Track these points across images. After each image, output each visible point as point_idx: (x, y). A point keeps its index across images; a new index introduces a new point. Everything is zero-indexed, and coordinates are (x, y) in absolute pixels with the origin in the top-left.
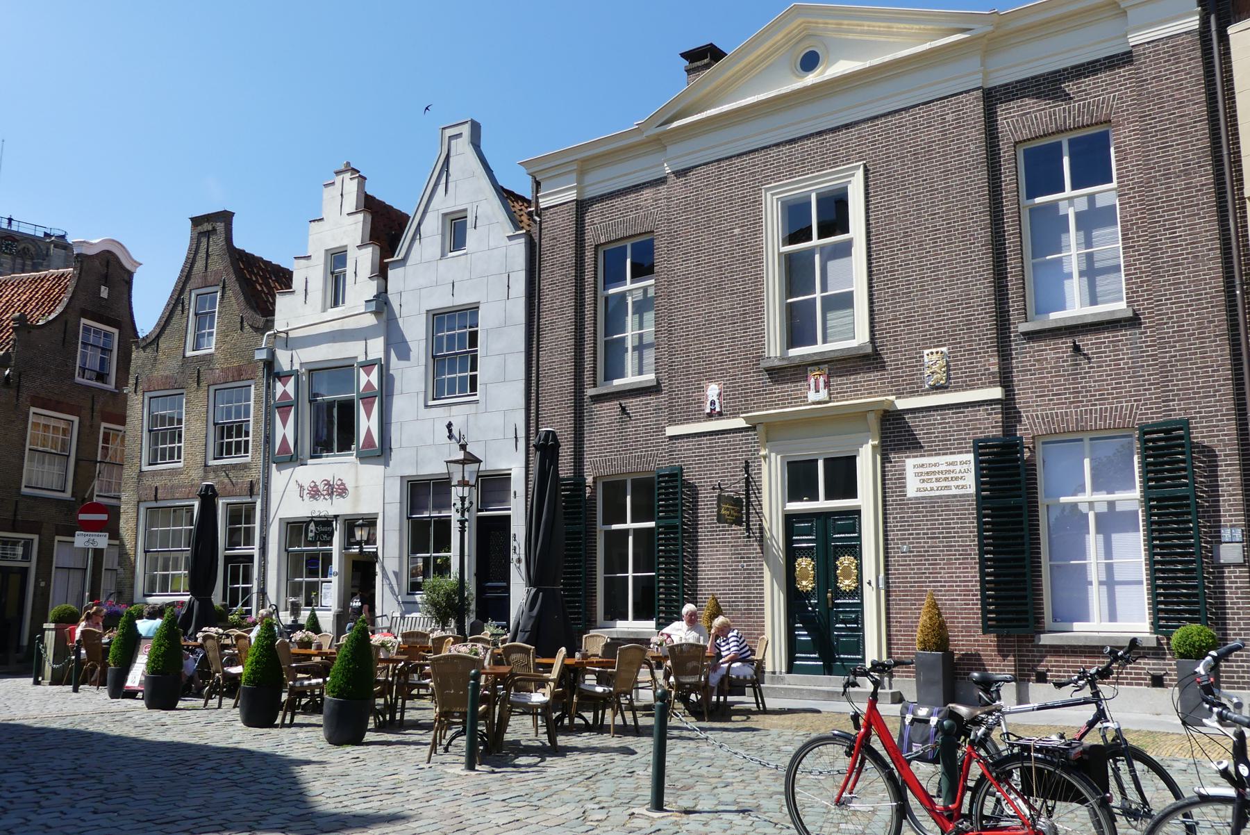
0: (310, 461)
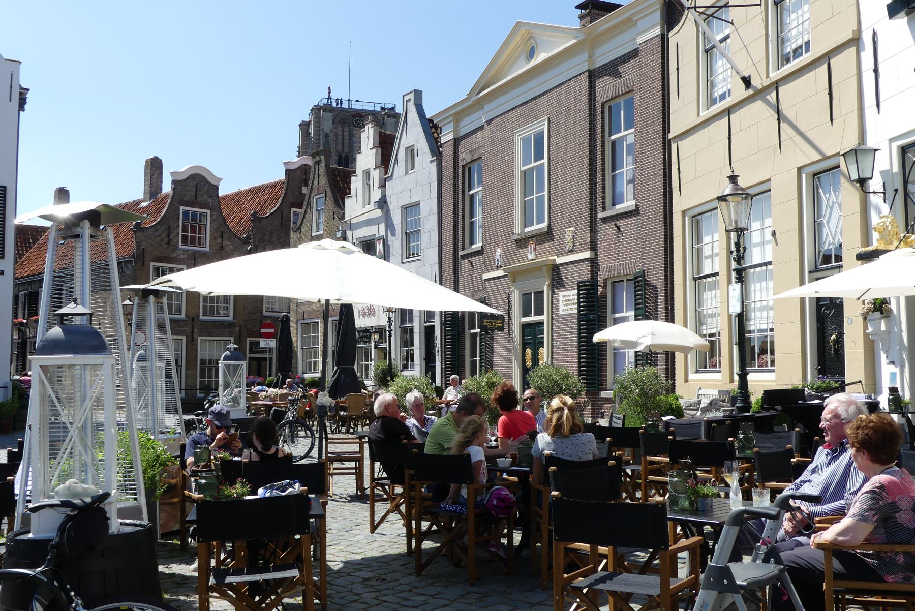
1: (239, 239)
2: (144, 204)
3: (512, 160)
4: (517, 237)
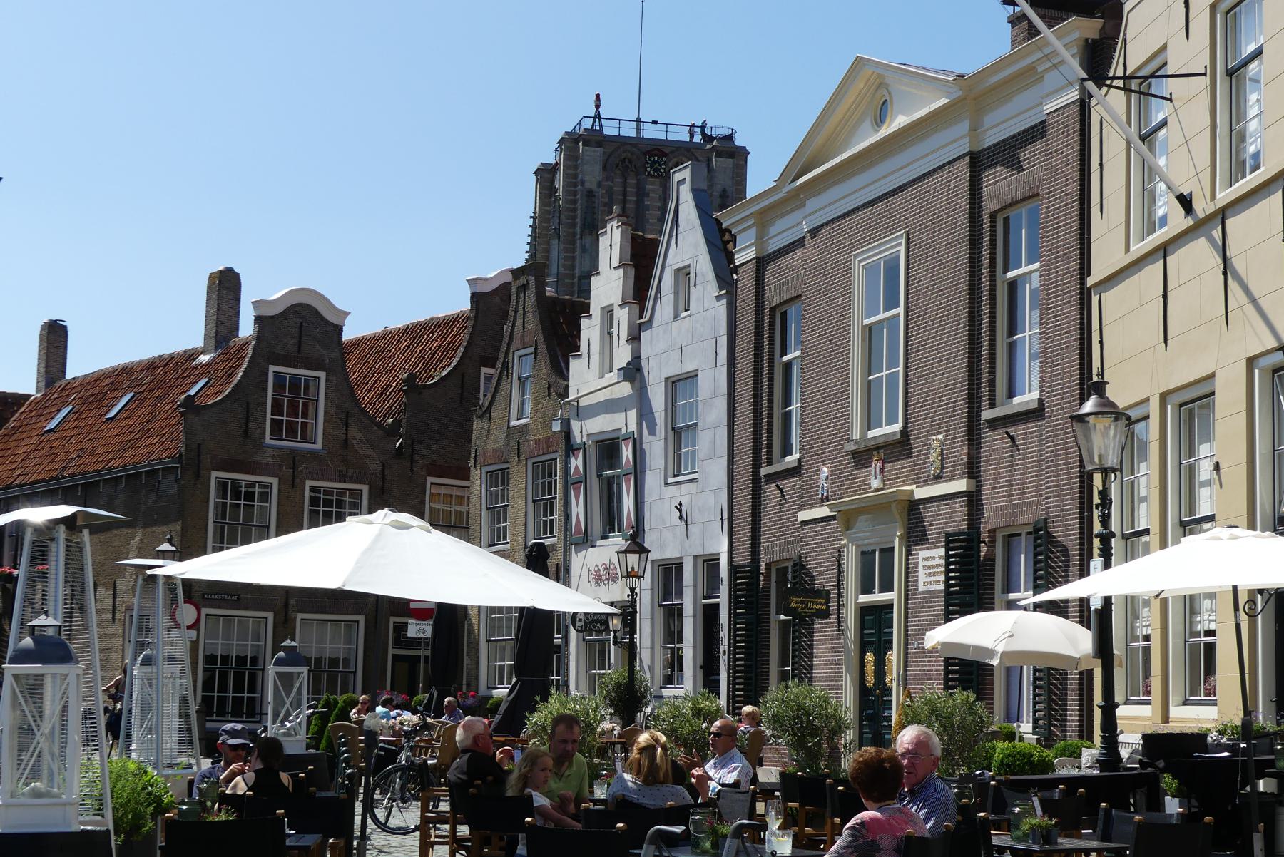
0: (599, 543)
1: (379, 425)
2: (204, 359)
3: (847, 304)
4: (852, 447)
